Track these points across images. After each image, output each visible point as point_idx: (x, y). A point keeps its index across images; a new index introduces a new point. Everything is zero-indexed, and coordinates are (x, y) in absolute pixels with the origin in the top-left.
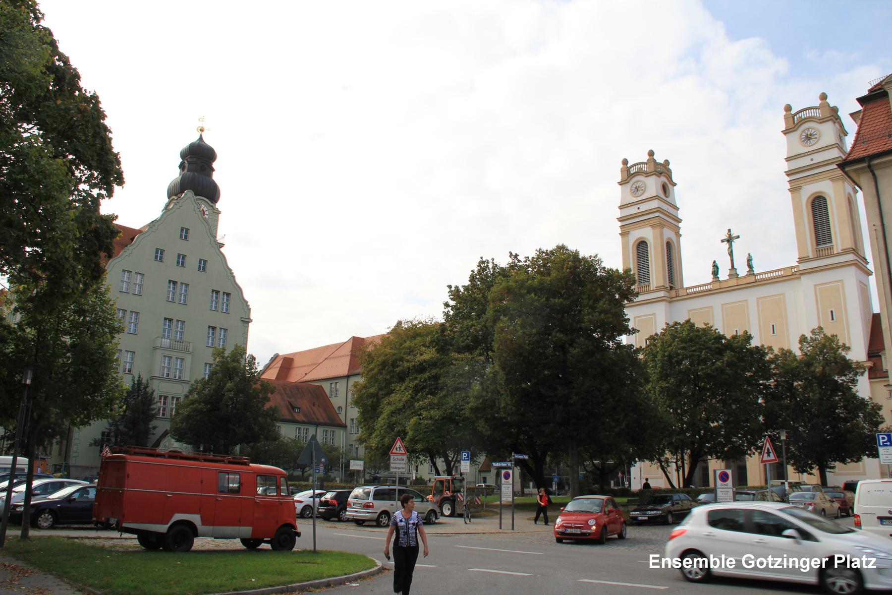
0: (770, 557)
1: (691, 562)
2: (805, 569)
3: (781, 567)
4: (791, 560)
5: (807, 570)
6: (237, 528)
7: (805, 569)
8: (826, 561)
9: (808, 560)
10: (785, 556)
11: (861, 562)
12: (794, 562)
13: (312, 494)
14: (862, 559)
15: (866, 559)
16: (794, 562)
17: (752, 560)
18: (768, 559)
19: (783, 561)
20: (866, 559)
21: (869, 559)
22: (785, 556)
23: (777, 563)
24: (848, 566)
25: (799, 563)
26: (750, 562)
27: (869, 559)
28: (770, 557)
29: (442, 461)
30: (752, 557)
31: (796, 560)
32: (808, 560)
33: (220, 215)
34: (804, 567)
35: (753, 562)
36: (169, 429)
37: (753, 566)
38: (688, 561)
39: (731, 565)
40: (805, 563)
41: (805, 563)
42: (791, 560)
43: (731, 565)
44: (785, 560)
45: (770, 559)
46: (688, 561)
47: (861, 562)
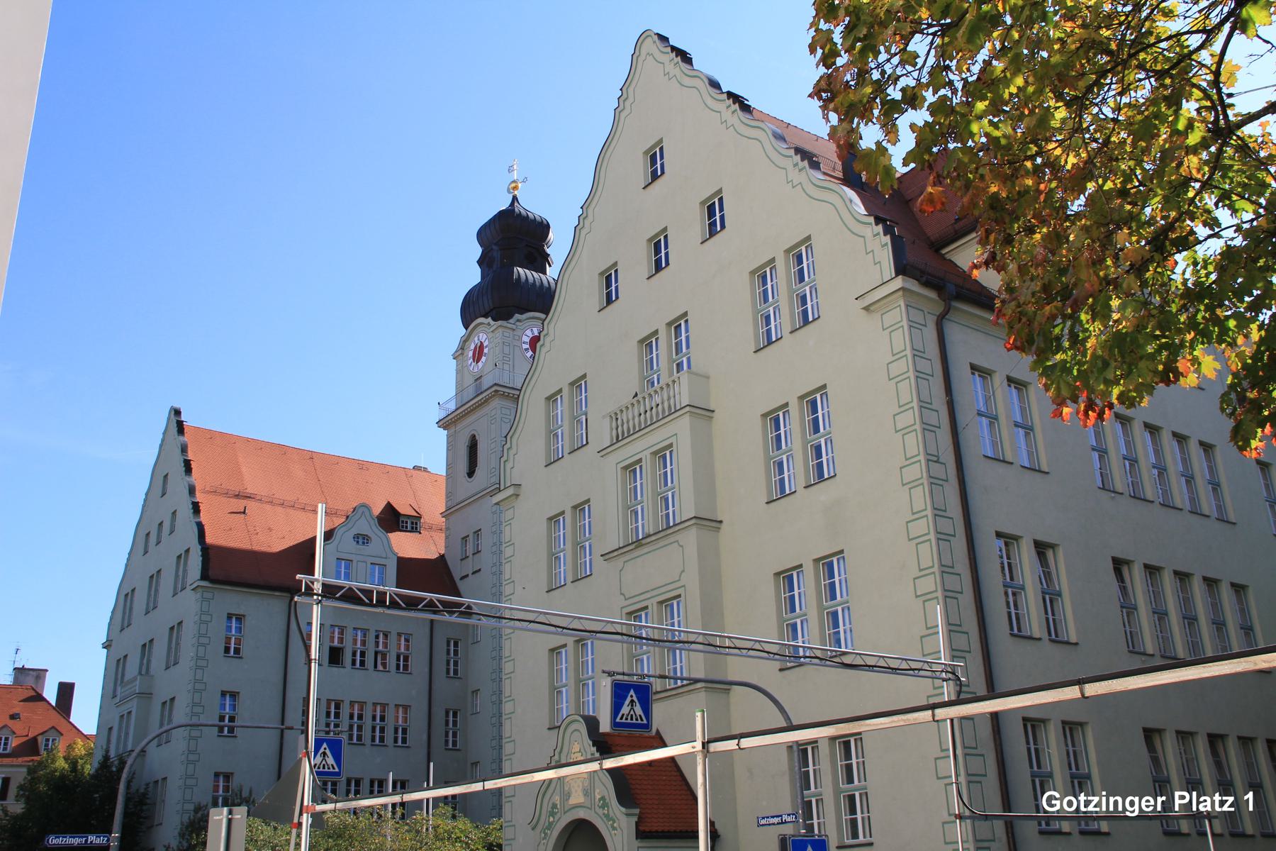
0: (1217, 794)
1: (1152, 802)
2: (1133, 812)
3: (1098, 809)
4: (1112, 800)
5: (1136, 814)
6: (1174, 767)
7: (1133, 812)
8: (1163, 801)
9: (1136, 799)
10: (1104, 793)
11: (1213, 803)
12: (1116, 803)
13: (333, 808)
14: (1214, 798)
15: (1085, 798)
16: (1116, 803)
17: (1056, 799)
18: (1214, 798)
19: (1101, 800)
20: (1085, 798)
21: (1224, 798)
22: (1104, 793)
23: (1093, 804)
24: (1194, 809)
25: (1079, 802)
26: (1054, 802)
27: (1224, 798)
28: (1217, 794)
29: (1215, 369)
30: (1057, 795)
31: (1119, 799)
32: (1136, 799)
33: (48, 673)
34: (1131, 809)
35: (1058, 803)
36: (1211, 357)
37: (1058, 807)
38: (1148, 801)
39: (1147, 806)
40: (1132, 803)
41: (1132, 803)
42: (1112, 800)
43: (1147, 806)
44: (1104, 799)
45: (1082, 798)
46: (1148, 801)
47: (1213, 803)
